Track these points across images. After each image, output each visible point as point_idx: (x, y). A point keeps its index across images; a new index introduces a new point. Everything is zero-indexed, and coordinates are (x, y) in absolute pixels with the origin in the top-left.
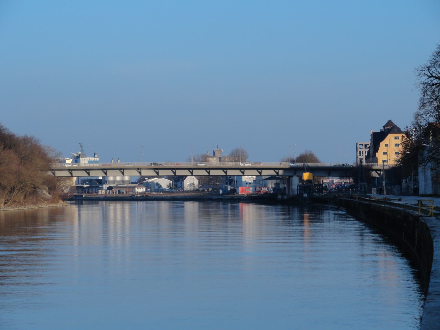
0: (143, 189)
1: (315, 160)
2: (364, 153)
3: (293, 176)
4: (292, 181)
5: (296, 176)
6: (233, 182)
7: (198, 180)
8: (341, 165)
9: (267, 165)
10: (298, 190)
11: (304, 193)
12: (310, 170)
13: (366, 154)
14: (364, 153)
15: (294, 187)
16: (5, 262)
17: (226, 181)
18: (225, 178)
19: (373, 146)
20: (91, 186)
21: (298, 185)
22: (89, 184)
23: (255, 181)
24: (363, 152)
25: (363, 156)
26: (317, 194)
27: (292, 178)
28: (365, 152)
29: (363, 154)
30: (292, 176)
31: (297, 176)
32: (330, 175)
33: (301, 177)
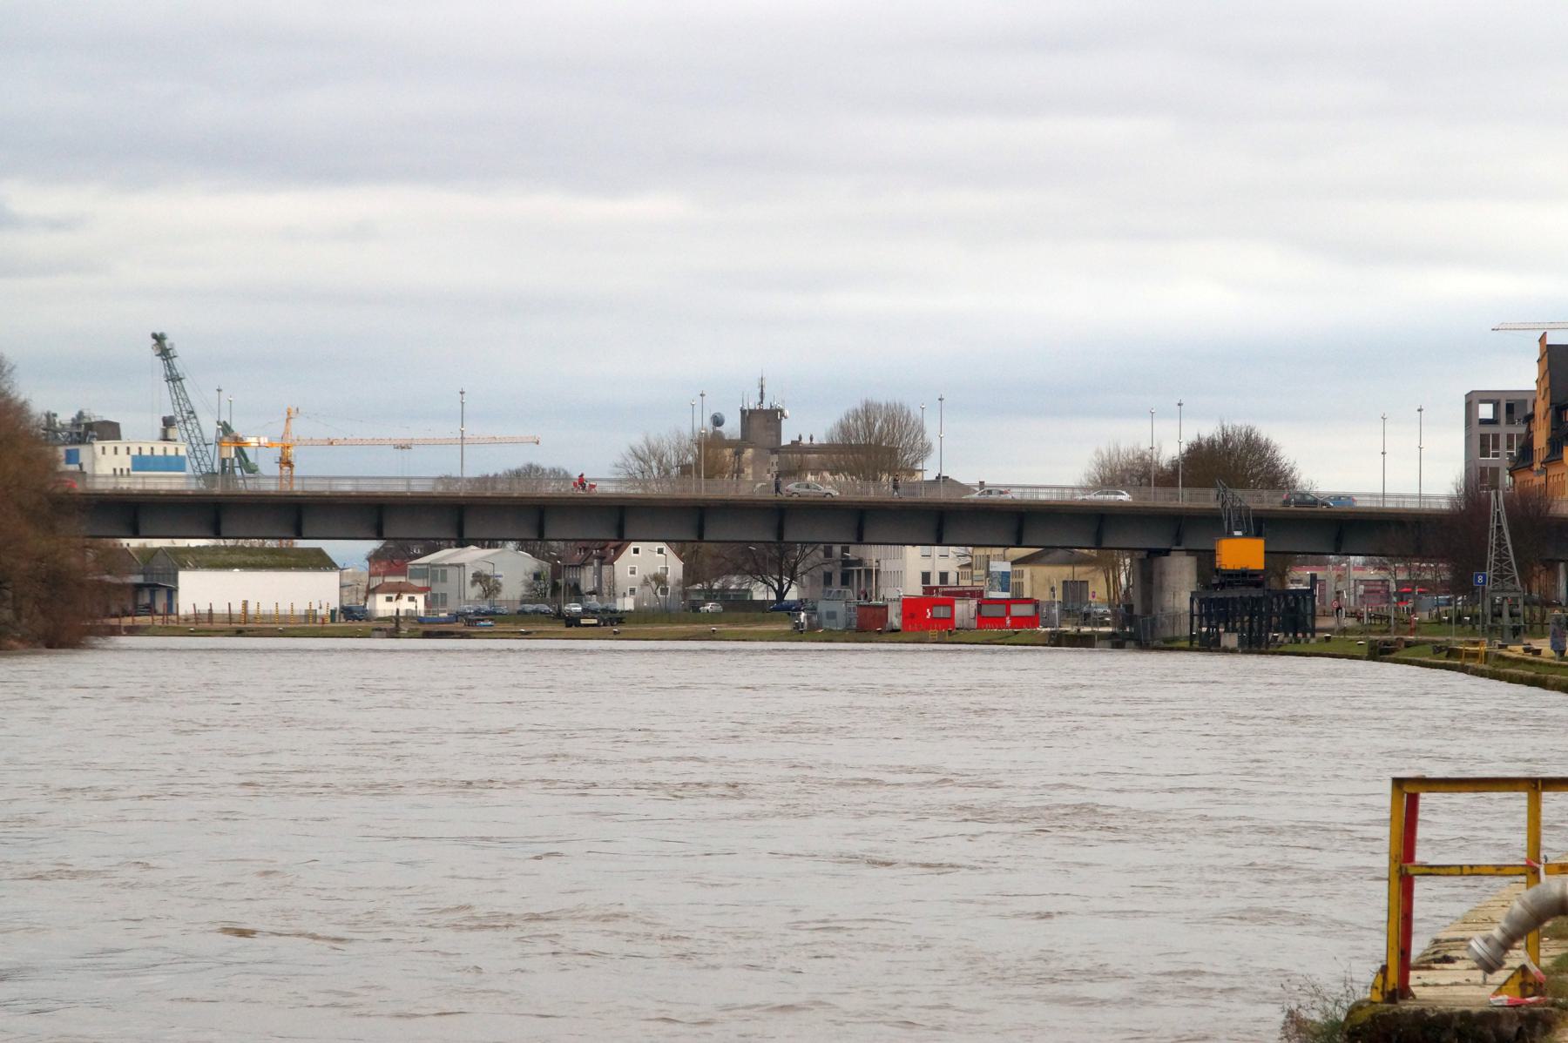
0: (411, 599)
1: (1275, 477)
2: (1503, 442)
3: (1167, 552)
4: (1162, 574)
5: (1185, 553)
6: (859, 571)
7: (682, 559)
8: (31, 417)
9: (914, 494)
10: (1192, 616)
11: (1221, 630)
12: (1259, 525)
13: (1510, 447)
14: (1503, 442)
15: (1171, 604)
16: (1454, 999)
17: (827, 568)
18: (822, 555)
19: (1550, 412)
20: (145, 580)
21: (1192, 593)
22: (1114, 626)
23: (969, 570)
24: (1496, 437)
25: (1496, 455)
26: (1286, 635)
27: (1166, 558)
28: (1510, 437)
29: (1496, 446)
30: (1164, 549)
31: (1189, 552)
32: (1343, 551)
33: (1206, 559)
